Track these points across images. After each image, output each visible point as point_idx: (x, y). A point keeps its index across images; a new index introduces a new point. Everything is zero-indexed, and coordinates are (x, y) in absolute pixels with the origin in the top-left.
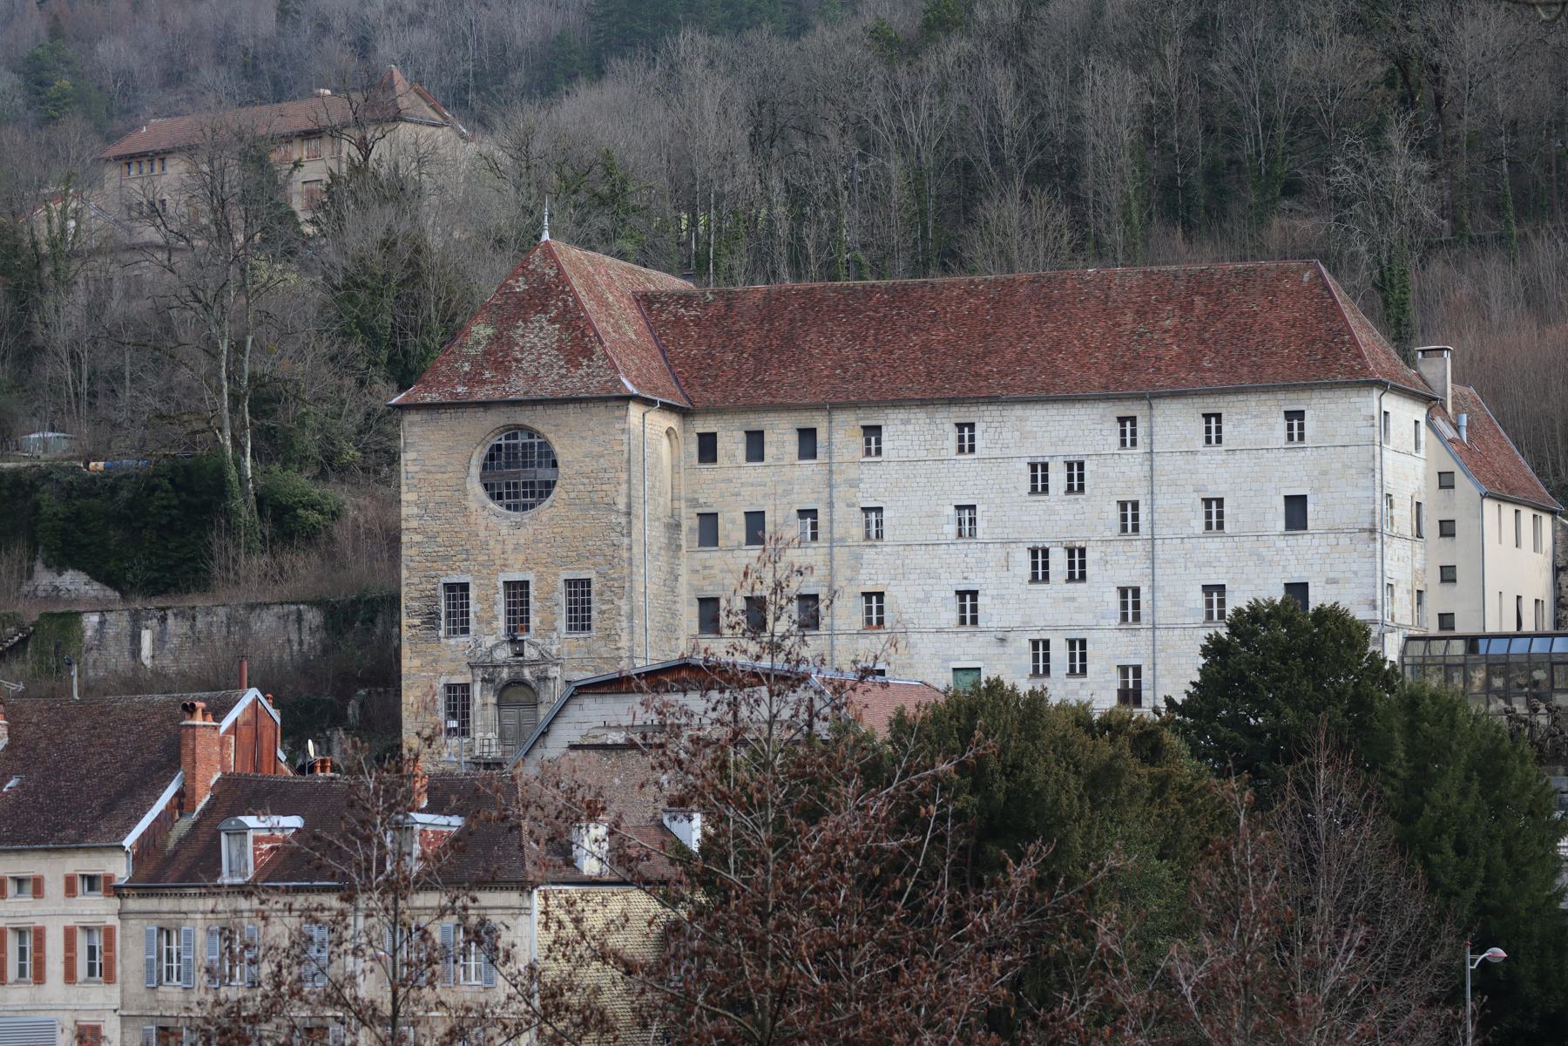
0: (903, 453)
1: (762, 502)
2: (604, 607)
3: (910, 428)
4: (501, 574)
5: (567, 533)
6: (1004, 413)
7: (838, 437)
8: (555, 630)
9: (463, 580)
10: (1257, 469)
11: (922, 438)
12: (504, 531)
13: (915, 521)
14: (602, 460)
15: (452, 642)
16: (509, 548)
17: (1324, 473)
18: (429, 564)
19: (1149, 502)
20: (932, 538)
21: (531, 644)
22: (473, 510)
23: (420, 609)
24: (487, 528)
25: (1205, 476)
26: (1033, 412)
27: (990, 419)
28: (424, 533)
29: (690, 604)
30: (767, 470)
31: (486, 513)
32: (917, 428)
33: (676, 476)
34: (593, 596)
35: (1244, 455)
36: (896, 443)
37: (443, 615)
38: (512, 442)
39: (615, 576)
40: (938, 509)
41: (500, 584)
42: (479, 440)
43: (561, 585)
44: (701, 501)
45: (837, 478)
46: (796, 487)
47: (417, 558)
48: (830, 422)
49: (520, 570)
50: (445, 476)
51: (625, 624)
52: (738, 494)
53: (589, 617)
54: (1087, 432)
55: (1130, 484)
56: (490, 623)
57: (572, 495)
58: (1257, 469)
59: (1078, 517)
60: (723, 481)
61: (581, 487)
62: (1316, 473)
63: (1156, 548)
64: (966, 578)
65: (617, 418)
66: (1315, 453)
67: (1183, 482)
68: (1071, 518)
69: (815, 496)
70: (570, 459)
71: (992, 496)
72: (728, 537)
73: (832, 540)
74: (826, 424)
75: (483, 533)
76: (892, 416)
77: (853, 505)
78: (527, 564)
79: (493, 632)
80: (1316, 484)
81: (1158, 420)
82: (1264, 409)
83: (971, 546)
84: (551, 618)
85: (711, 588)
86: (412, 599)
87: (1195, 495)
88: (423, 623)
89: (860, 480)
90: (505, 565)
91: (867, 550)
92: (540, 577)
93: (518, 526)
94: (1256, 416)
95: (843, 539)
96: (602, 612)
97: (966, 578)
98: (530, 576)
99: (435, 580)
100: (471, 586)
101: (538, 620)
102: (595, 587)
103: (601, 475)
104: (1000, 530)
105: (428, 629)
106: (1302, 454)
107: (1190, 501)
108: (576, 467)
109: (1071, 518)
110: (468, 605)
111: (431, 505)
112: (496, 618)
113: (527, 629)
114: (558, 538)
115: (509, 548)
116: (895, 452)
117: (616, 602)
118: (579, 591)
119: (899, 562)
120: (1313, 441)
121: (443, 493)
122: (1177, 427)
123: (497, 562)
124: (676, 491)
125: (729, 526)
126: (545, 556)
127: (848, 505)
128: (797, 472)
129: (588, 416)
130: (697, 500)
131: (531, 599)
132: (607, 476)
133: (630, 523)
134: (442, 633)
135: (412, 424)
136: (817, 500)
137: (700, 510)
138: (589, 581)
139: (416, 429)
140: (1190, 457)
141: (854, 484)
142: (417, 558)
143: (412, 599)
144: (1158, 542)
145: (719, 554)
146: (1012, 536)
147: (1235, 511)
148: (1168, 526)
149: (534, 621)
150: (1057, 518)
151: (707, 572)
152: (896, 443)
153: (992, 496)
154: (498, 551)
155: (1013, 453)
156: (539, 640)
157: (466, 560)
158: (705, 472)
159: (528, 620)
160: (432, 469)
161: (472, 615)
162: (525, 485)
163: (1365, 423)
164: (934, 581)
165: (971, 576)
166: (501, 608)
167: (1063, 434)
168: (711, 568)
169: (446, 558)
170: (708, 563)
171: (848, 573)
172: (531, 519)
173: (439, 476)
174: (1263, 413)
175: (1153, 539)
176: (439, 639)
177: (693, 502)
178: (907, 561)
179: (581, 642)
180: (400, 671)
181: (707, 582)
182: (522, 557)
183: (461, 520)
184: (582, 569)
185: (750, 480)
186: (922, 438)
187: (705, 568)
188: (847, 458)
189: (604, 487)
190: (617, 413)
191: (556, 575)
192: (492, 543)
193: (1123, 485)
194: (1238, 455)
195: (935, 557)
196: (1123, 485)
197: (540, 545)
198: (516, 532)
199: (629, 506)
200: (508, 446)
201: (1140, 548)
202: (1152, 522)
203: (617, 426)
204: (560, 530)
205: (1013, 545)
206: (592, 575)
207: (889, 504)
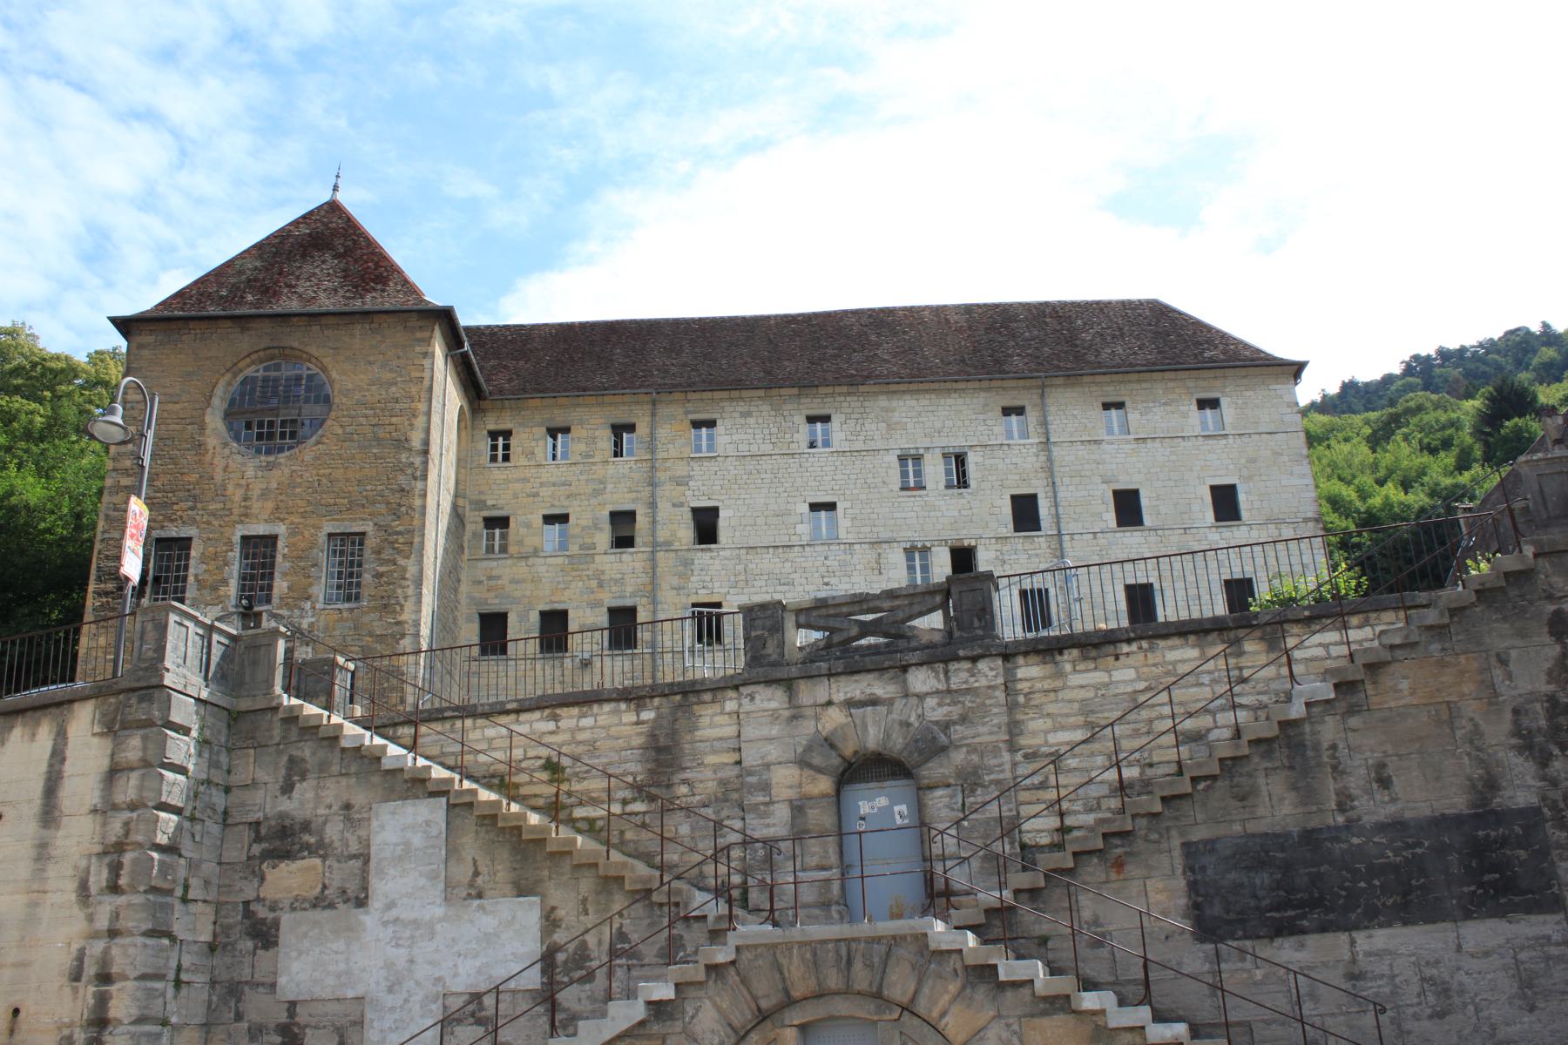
0: (744, 448)
1: (566, 503)
2: (382, 569)
3: (751, 421)
4: (239, 526)
5: (338, 474)
6: (866, 404)
7: (663, 433)
8: (308, 598)
10: (1173, 458)
11: (766, 431)
12: (250, 473)
13: (760, 521)
14: (394, 389)
16: (256, 493)
17: (1252, 461)
19: (1051, 494)
20: (784, 540)
22: (210, 447)
24: (225, 469)
25: (1114, 466)
26: (901, 403)
27: (850, 410)
29: (468, 620)
30: (574, 468)
31: (227, 451)
32: (760, 421)
33: (463, 471)
34: (368, 554)
35: (1157, 444)
36: (735, 437)
38: (273, 374)
39: (400, 528)
40: (788, 507)
41: (236, 539)
42: (229, 365)
44: (489, 503)
45: (661, 476)
46: (610, 487)
48: (653, 415)
49: (266, 521)
50: (178, 406)
51: (410, 591)
52: (536, 495)
53: (358, 585)
54: (967, 423)
55: (1025, 476)
56: (214, 589)
57: (348, 429)
58: (1173, 458)
59: (963, 512)
60: (518, 481)
62: (1243, 461)
63: (1065, 545)
64: (827, 584)
65: (419, 340)
66: (1238, 441)
67: (1088, 473)
68: (956, 513)
69: (634, 495)
70: (350, 386)
71: (857, 491)
72: (520, 543)
73: (655, 544)
74: (648, 419)
75: (219, 476)
76: (727, 406)
77: (681, 505)
78: (276, 516)
79: (220, 600)
80: (1245, 473)
81: (1052, 409)
82: (1174, 396)
83: (832, 547)
85: (497, 601)
87: (1105, 486)
89: (690, 476)
90: (246, 515)
91: (699, 554)
92: (294, 531)
93: (270, 467)
94: (1165, 404)
95: (668, 543)
96: (379, 575)
97: (827, 584)
98: (281, 529)
101: (285, 584)
102: (371, 542)
104: (869, 529)
106: (1224, 442)
107: (1099, 493)
108: (358, 396)
109: (956, 513)
110: (186, 567)
112: (225, 582)
113: (269, 601)
114: (324, 481)
115: (256, 493)
116: (732, 446)
117: (402, 562)
118: (348, 545)
119: (740, 568)
120: (1233, 428)
121: (171, 427)
122: (1075, 416)
123: (236, 511)
124: (461, 487)
125: (523, 531)
127: (674, 505)
128: (611, 469)
129: (379, 338)
130: (484, 502)
131: (279, 559)
133: (426, 463)
136: (634, 501)
137: (487, 514)
139: (146, 352)
140: (1094, 447)
141: (682, 482)
144: (1066, 538)
145: (509, 562)
146: (885, 535)
147: (1155, 503)
148: (1075, 520)
149: (280, 586)
150: (940, 514)
151: (493, 583)
152: (735, 437)
153: (857, 491)
154: (237, 498)
155: (879, 445)
156: (284, 612)
157: (192, 509)
158: (496, 472)
159: (270, 587)
161: (191, 579)
162: (283, 423)
163: (1289, 410)
164: (786, 588)
165: (833, 581)
166: (234, 571)
167: (938, 425)
168: (498, 578)
170: (495, 573)
171: (675, 581)
172: (288, 458)
174: (1173, 401)
175: (1059, 534)
177: (480, 505)
178: (751, 566)
179: (345, 614)
181: (492, 594)
182: (270, 505)
184: (354, 520)
185: (551, 480)
186: (766, 431)
187: (490, 578)
188: (673, 452)
189: (394, 420)
190: (419, 335)
191: (318, 528)
192: (230, 488)
193: (1017, 477)
194: (1150, 444)
195: (787, 560)
196: (1017, 477)
197: (298, 490)
199: (426, 442)
200: (266, 380)
201: (1044, 545)
202: (1057, 516)
203: (418, 349)
204: (328, 471)
205: (884, 546)
206: (368, 528)
207: (727, 502)
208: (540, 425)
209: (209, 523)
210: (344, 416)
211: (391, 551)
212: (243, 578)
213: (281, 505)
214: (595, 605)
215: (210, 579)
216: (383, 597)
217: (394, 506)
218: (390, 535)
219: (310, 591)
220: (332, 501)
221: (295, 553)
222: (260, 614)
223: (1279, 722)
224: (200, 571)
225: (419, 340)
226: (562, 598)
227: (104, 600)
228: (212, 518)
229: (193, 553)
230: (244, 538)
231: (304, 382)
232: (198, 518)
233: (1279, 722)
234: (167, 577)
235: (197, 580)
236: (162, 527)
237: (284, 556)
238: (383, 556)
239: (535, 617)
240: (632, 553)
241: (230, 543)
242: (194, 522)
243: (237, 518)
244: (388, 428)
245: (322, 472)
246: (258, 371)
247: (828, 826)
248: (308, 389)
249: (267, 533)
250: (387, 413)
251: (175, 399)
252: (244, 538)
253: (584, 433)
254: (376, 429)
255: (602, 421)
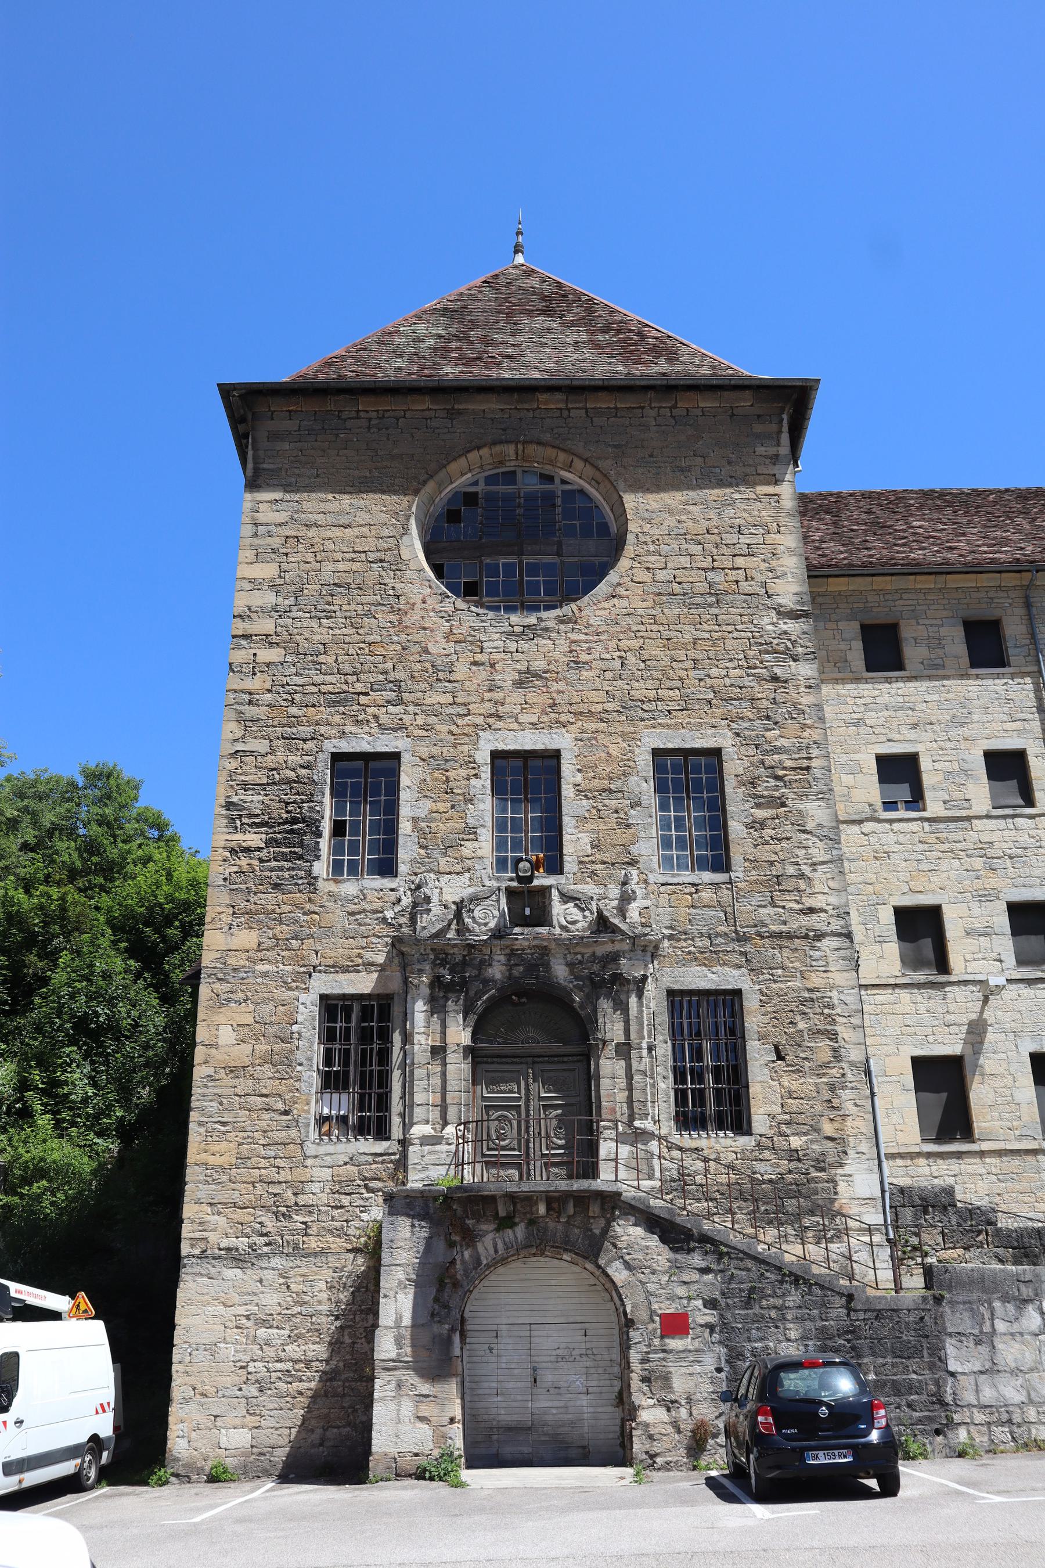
2: (761, 814)
14: (730, 512)
39: (781, 742)
41: (483, 757)
52: (858, 723)
57: (661, 575)
98: (562, 740)
101: (585, 839)
102: (733, 767)
114: (631, 659)
121: (340, 567)
125: (847, 780)
191: (631, 738)
197: (585, 674)
203: (760, 450)
206: (723, 739)
208: (851, 617)
209: (424, 727)
210: (649, 553)
211: (773, 782)
212: (500, 825)
214: (985, 897)
216: (772, 863)
217: (765, 703)
218: (766, 752)
220: (651, 694)
222: (545, 891)
223: (671, 993)
226: (929, 886)
227: (244, 862)
228: (433, 720)
229: (405, 780)
230: (496, 755)
231: (559, 501)
232: (407, 719)
233: (671, 993)
234: (355, 824)
235: (416, 828)
236: (343, 734)
237: (579, 790)
239: (887, 916)
240: (1032, 817)
241: (471, 763)
242: (400, 727)
243: (479, 721)
244: (733, 575)
245: (624, 644)
246: (476, 483)
249: (539, 747)
250: (724, 550)
251: (345, 520)
252: (496, 755)
253: (921, 631)
254: (710, 575)
255: (945, 613)
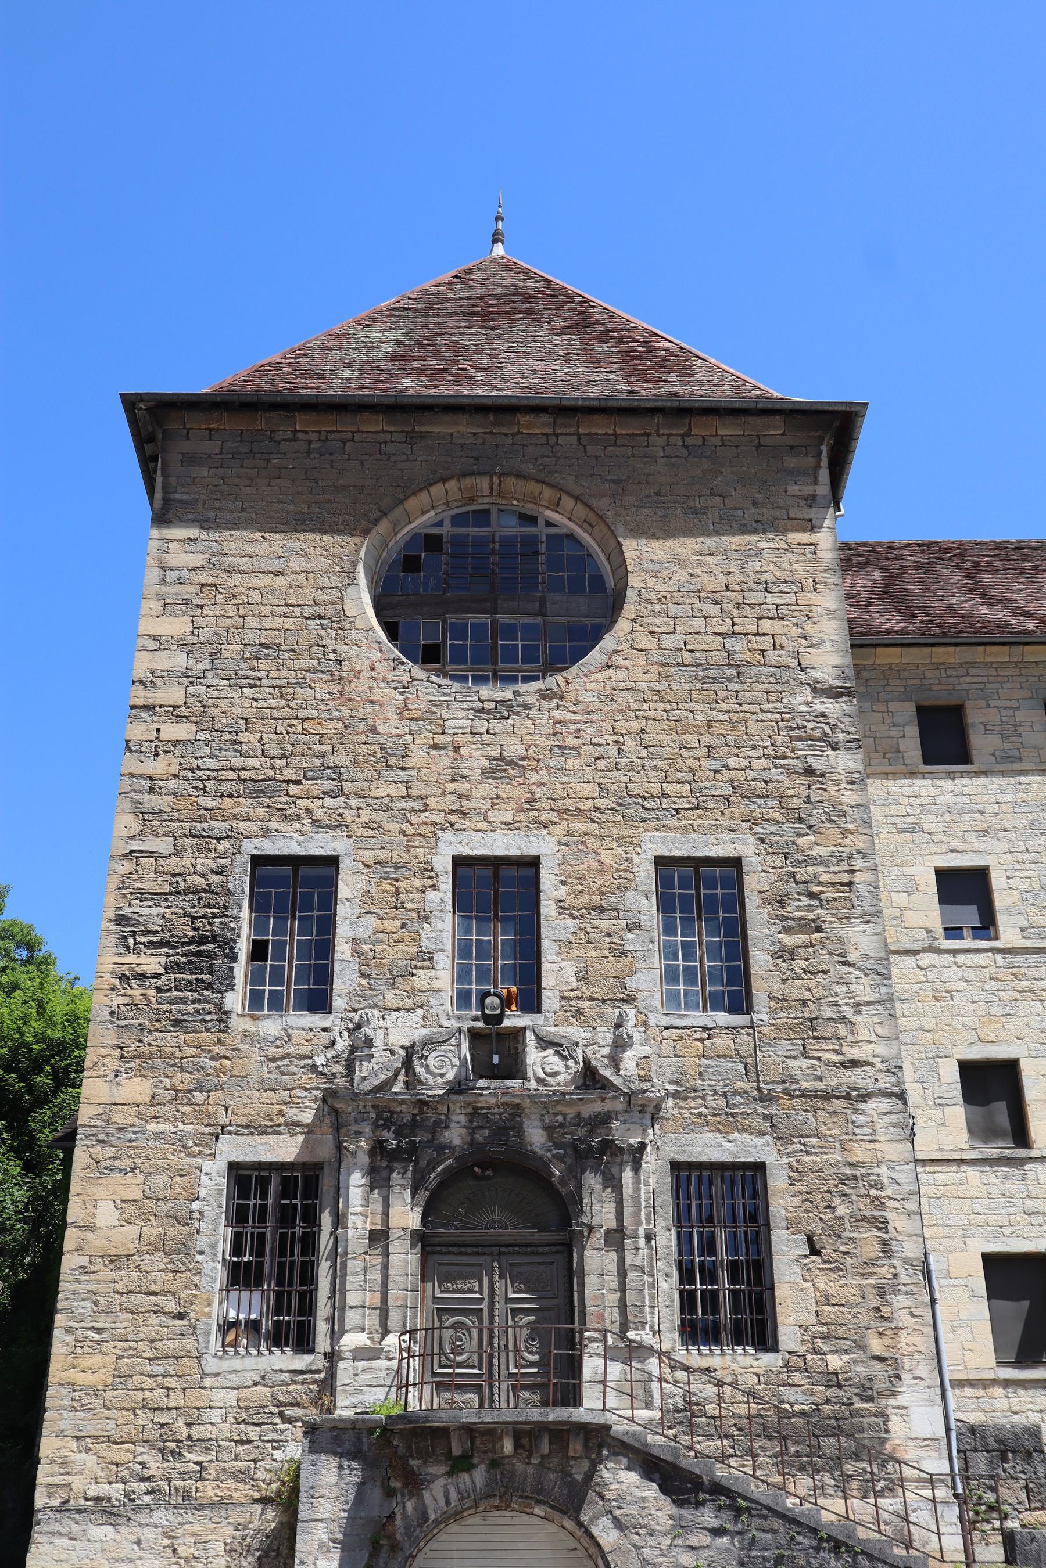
2: (791, 940)
4: (446, 836)
5: (658, 733)
8: (629, 999)
9: (319, 845)
14: (754, 564)
15: (271, 1026)
18: (206, 802)
21: (544, 1043)
23: (167, 925)
28: (203, 718)
37: (243, 949)
38: (473, 531)
41: (443, 864)
43: (645, 873)
47: (173, 784)
57: (669, 641)
61: (698, 625)
65: (791, 472)
84: (614, 966)
86: (141, 895)
88: (172, 967)
99: (225, 845)
100: (345, 864)
101: (570, 969)
103: (754, 598)
105: (189, 986)
108: (682, 575)
111: (232, 649)
112: (427, 958)
114: (630, 744)
121: (269, 623)
125: (900, 899)
126: (591, 790)
132: (771, 599)
134: (235, 1000)
135: (190, 460)
138: (736, 862)
142: (173, 784)
143: (141, 895)
156: (574, 1032)
160: (245, 563)
169: (259, 789)
172: (543, 695)
173: (265, 581)
176: (223, 1016)
180: (233, 525)
183: (322, 688)
189: (766, 626)
191: (629, 843)
192: (418, 755)
198: (497, 726)
203: (793, 489)
208: (905, 697)
209: (371, 826)
210: (654, 614)
211: (806, 901)
212: (463, 950)
213: (539, 793)
215: (393, 953)
216: (804, 1003)
217: (797, 802)
218: (798, 864)
219: (631, 983)
220: (655, 789)
221: (584, 899)
224: (364, 933)
225: (791, 472)
227: (137, 991)
228: (380, 816)
230: (459, 862)
231: (542, 548)
232: (349, 815)
234: (280, 946)
235: (357, 952)
236: (267, 833)
237: (562, 908)
238: (790, 910)
242: (339, 824)
243: (439, 818)
244: (757, 643)
245: (621, 726)
246: (440, 524)
247: (958, 1547)
248: (554, 564)
250: (747, 611)
251: (275, 566)
252: (459, 862)
253: (993, 716)
